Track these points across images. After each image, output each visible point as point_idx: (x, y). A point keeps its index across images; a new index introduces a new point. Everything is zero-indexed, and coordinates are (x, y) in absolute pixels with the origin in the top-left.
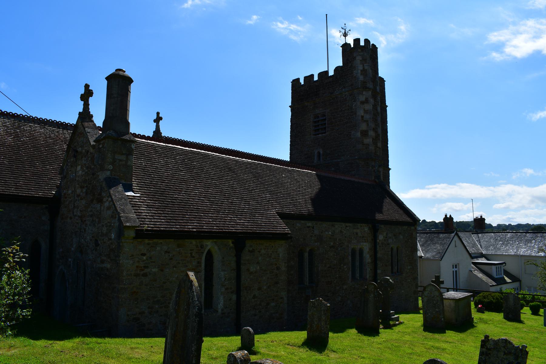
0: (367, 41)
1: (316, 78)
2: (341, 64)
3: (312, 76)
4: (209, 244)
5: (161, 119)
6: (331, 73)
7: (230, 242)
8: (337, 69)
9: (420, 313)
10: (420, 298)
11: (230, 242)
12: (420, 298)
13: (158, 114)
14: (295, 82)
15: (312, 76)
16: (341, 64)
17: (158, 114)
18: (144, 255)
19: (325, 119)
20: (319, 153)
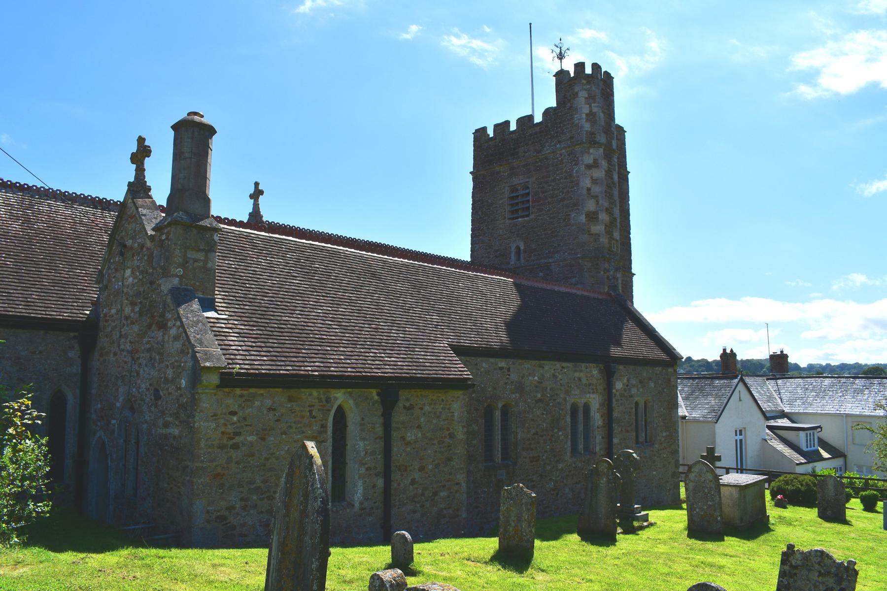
0: (596, 67)
1: (513, 127)
2: (553, 103)
4: (339, 396)
5: (262, 193)
6: (538, 119)
8: (547, 113)
10: (682, 484)
12: (682, 484)
14: (480, 134)
16: (553, 103)
17: (257, 184)
18: (233, 413)
20: (518, 248)
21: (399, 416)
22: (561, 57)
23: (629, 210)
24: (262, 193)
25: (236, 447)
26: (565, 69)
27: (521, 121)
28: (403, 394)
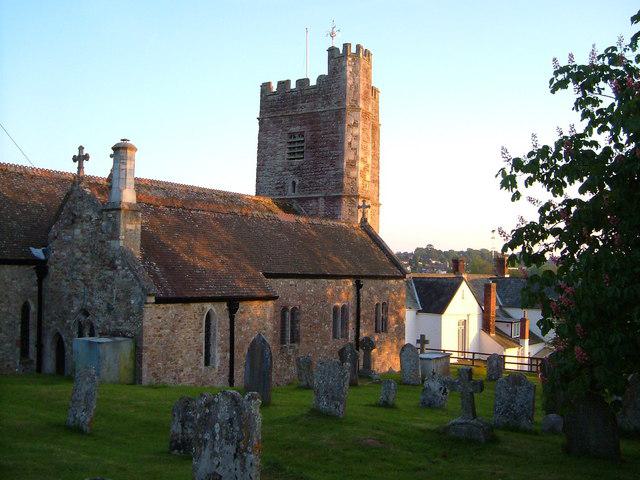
0: (358, 47)
1: (293, 86)
2: (325, 72)
3: (288, 82)
4: (208, 306)
5: (86, 157)
6: (313, 82)
7: (225, 306)
8: (320, 79)
9: (141, 185)
10: (361, 367)
11: (225, 306)
12: (361, 367)
13: (81, 148)
14: (265, 87)
15: (288, 82)
16: (325, 72)
17: (81, 148)
18: (159, 318)
19: (303, 141)
20: (294, 183)
21: (238, 317)
22: (332, 35)
23: (188, 190)
24: (86, 157)
25: (160, 336)
26: (336, 46)
27: (300, 82)
28: (241, 305)
